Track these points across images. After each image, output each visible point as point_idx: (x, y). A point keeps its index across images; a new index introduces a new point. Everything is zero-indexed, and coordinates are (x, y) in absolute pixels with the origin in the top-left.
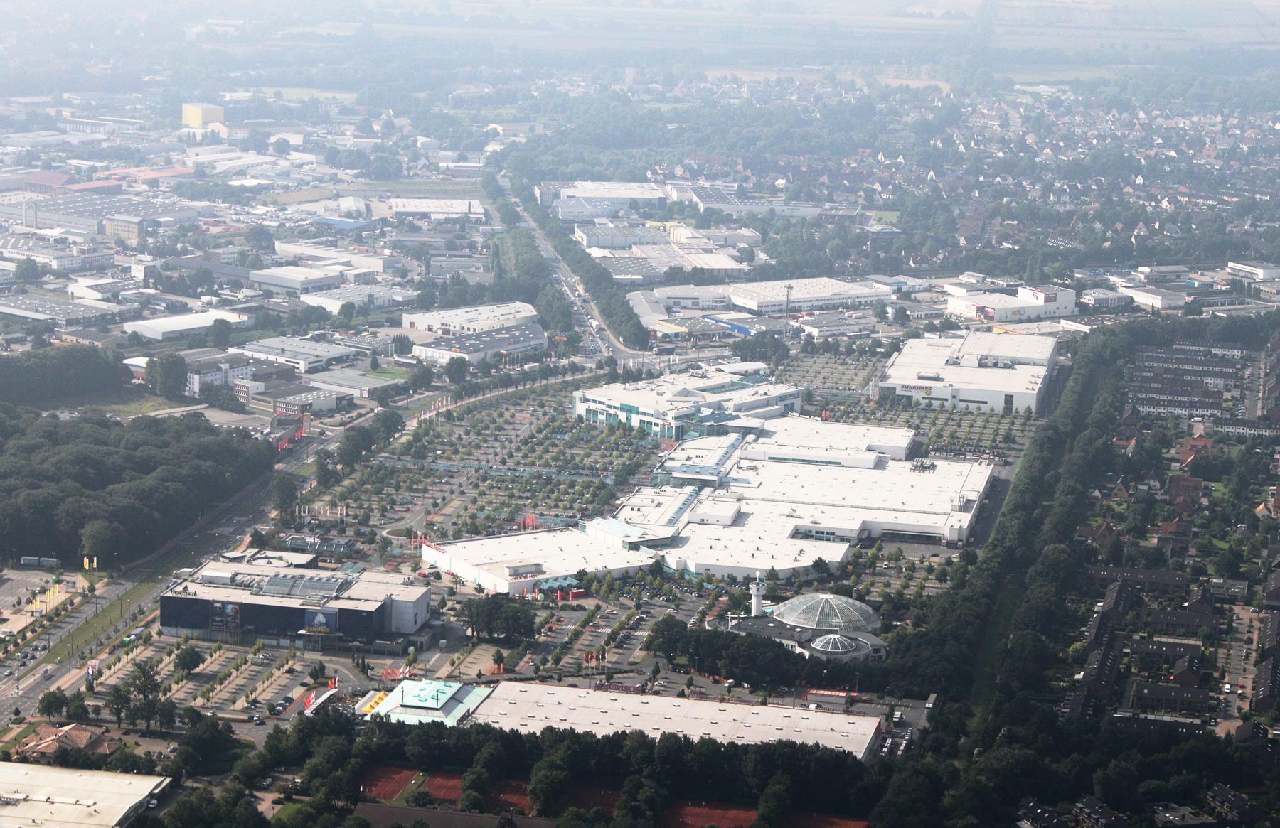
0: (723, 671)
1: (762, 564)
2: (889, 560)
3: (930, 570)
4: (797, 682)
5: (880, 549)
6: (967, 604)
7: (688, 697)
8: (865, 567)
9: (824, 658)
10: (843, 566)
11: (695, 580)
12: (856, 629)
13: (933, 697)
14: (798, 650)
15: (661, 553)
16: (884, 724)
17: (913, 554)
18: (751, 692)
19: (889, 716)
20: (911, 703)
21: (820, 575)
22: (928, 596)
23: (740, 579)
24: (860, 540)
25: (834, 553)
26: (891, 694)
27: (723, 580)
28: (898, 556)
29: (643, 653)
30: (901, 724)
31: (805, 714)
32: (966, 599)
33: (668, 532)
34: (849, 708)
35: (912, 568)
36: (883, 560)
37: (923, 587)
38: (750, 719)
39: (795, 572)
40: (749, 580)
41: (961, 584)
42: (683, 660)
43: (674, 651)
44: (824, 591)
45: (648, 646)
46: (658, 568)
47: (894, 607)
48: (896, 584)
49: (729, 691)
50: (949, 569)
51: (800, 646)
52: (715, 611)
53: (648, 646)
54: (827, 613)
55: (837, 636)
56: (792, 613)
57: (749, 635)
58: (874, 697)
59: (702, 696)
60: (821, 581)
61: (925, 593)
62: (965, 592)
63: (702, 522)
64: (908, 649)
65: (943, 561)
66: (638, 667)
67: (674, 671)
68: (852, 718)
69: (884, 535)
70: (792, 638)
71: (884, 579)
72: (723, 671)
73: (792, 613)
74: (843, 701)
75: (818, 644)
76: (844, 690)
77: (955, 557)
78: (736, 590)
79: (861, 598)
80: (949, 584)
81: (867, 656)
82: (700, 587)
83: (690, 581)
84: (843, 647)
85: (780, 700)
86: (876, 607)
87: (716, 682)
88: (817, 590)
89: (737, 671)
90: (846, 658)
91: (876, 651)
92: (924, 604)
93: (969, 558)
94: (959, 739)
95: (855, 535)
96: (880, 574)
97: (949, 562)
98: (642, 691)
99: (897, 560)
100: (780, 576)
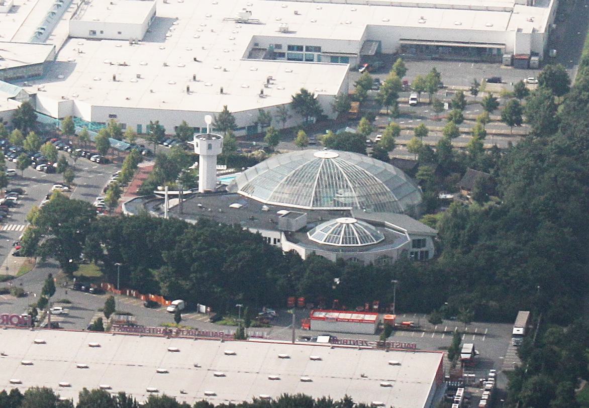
0: (164, 287)
1: (205, 105)
2: (419, 90)
3: (491, 105)
4: (291, 301)
5: (401, 72)
6: (564, 158)
7: (108, 330)
8: (379, 103)
9: (333, 257)
10: (344, 102)
11: (94, 135)
12: (380, 207)
13: (523, 317)
14: (286, 246)
15: (31, 90)
16: (447, 363)
17: (459, 79)
18: (214, 320)
19: (454, 351)
20: (486, 328)
21: (307, 119)
22: (495, 149)
23: (170, 131)
24: (364, 58)
25: (328, 82)
26: (451, 314)
27: (140, 134)
28: (435, 84)
29: (21, 260)
30: (474, 363)
31: (316, 352)
32: (561, 151)
33: (38, 55)
34: (385, 336)
35: (460, 103)
36: (408, 89)
37: (483, 135)
38: (223, 364)
39: (264, 117)
40: (185, 133)
41: (549, 126)
42: (90, 270)
43: (76, 257)
44: (316, 144)
45: (29, 248)
46: (27, 116)
47: (438, 170)
48: (436, 134)
49: (178, 320)
50: (523, 102)
51: (290, 238)
52: (135, 184)
53: (29, 248)
54: (331, 180)
55: (350, 220)
56: (269, 184)
57: (203, 223)
58: (423, 320)
59: (131, 328)
60: (310, 129)
61: (488, 145)
62: (558, 138)
63: (93, 36)
64: (473, 238)
65: (511, 89)
66: (15, 284)
67: (78, 288)
68: (395, 356)
69: (404, 48)
70: (274, 226)
71: (417, 124)
72: (164, 287)
73: (269, 184)
74: (372, 328)
75: (320, 235)
76: (370, 311)
77: (531, 81)
78: (168, 149)
79: (381, 154)
80: (525, 128)
81: (404, 250)
82: (105, 146)
83: (84, 138)
84: (364, 238)
85: (264, 331)
86: (410, 170)
87: (152, 305)
88: (303, 145)
89: (185, 284)
90: (369, 257)
91: (418, 243)
92: (493, 162)
93: (556, 83)
94: (576, 384)
95: (356, 49)
96: (407, 115)
97: (521, 91)
98: (30, 323)
99: (432, 91)
100: (239, 123)
